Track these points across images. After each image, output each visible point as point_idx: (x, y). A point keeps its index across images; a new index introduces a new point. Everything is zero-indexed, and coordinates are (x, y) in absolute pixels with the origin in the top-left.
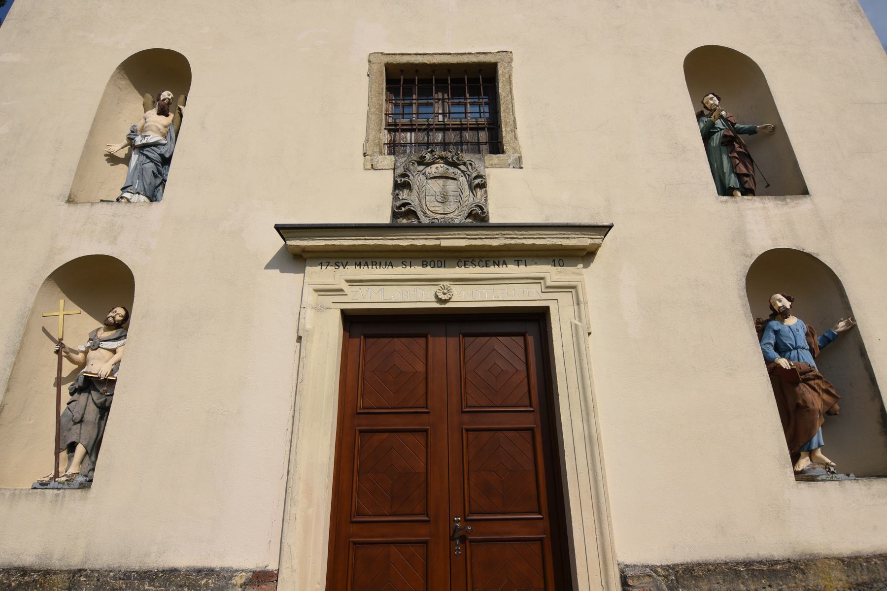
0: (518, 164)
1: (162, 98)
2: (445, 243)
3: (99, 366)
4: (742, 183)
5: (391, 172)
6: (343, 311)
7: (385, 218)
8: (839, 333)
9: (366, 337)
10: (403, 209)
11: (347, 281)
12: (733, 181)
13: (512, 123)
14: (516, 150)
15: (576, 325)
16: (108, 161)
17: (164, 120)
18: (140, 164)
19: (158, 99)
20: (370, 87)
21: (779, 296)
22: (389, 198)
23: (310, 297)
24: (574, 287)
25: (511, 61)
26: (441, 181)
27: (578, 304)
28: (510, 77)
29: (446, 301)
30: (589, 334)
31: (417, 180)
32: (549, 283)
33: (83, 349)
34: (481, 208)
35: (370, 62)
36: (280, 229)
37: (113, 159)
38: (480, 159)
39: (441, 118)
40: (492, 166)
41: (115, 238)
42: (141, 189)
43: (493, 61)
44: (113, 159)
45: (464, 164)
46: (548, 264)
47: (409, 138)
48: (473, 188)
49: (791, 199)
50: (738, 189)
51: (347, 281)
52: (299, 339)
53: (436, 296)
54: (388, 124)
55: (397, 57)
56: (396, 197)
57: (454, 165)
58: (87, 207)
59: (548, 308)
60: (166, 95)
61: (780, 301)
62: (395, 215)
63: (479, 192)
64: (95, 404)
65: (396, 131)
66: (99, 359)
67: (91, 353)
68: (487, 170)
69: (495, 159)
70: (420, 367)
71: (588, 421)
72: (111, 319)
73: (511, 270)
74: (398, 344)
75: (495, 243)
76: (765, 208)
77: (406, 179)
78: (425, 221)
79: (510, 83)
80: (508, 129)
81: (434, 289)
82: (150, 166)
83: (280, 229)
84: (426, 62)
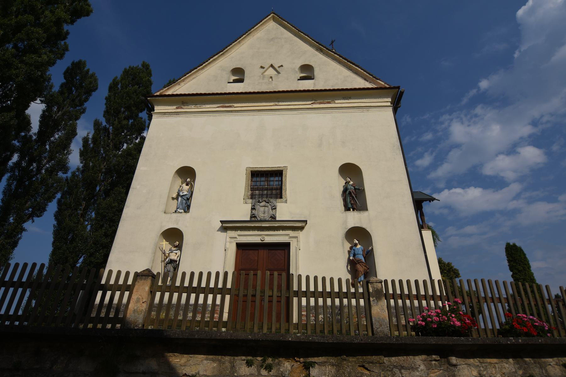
0: (286, 202)
1: (187, 181)
2: (263, 225)
3: (173, 257)
4: (352, 206)
5: (251, 204)
6: (236, 243)
7: (248, 219)
8: (370, 250)
9: (268, 250)
10: (253, 215)
11: (238, 235)
12: (350, 206)
13: (285, 189)
14: (286, 198)
15: (296, 247)
16: (172, 199)
17: (188, 187)
18: (181, 201)
19: (186, 181)
20: (246, 178)
21: (355, 240)
22: (250, 212)
23: (228, 239)
24: (297, 237)
25: (287, 169)
26: (264, 208)
27: (298, 242)
28: (286, 175)
29: (263, 241)
30: (300, 250)
31: (257, 207)
32: (290, 236)
33: (168, 253)
34: (274, 215)
35: (246, 170)
36: (221, 221)
37: (173, 199)
38: (275, 200)
39: (266, 186)
40: (279, 202)
41: (178, 223)
42: (182, 208)
43: (282, 169)
44: (173, 199)
45: (271, 202)
46: (291, 230)
47: (257, 192)
48: (272, 209)
49: (362, 212)
50: (351, 208)
51: (238, 235)
52: (225, 250)
53: (261, 239)
54: (251, 188)
55: (254, 168)
56: (252, 212)
57: (268, 203)
58: (170, 214)
59: (290, 242)
60: (188, 180)
61: (355, 241)
62: (251, 217)
63: (274, 211)
64: (173, 267)
65: (253, 190)
66: (173, 255)
67: (171, 254)
68: (277, 204)
69: (279, 200)
70: (256, 258)
71: (296, 272)
72: (175, 245)
73: (281, 232)
74: (251, 252)
75: (276, 225)
76: (354, 215)
77: (254, 207)
78: (259, 219)
79: (286, 177)
80: (284, 191)
81: (260, 237)
82: (184, 201)
83: (221, 221)
84: (262, 170)
